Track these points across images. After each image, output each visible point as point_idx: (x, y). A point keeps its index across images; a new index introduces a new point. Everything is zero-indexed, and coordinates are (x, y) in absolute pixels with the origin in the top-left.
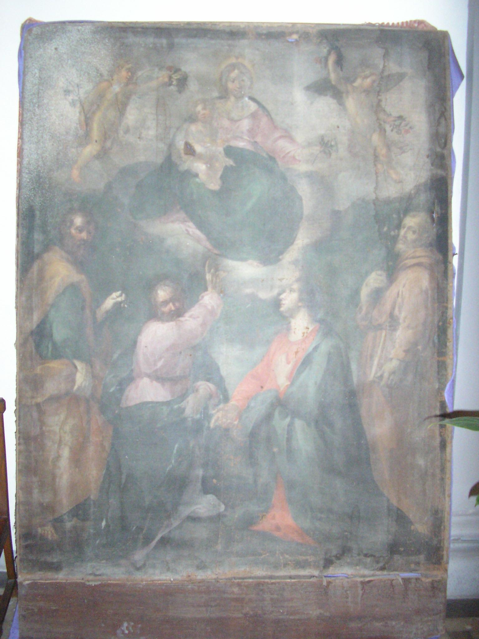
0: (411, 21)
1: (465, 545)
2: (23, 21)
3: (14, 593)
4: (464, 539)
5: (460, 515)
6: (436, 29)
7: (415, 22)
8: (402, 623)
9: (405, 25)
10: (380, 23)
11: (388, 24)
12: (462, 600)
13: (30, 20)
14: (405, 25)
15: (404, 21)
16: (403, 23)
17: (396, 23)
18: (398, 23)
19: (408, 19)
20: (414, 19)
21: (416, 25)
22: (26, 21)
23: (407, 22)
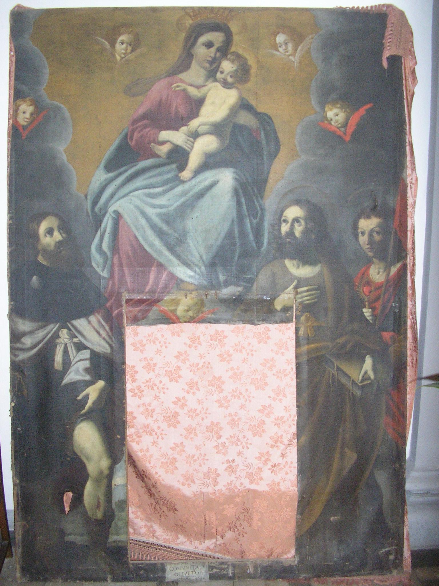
0: (379, 5)
1: (434, 498)
2: (11, 8)
3: (8, 553)
4: (434, 493)
5: (431, 470)
6: (342, 8)
7: (383, 5)
8: (217, 494)
9: (374, 9)
10: (351, 7)
11: (358, 7)
12: (430, 550)
13: (19, 6)
14: (374, 9)
15: (373, 5)
16: (372, 7)
17: (365, 6)
18: (367, 7)
19: (377, 4)
20: (382, 3)
21: (385, 9)
22: (14, 8)
23: (376, 6)
